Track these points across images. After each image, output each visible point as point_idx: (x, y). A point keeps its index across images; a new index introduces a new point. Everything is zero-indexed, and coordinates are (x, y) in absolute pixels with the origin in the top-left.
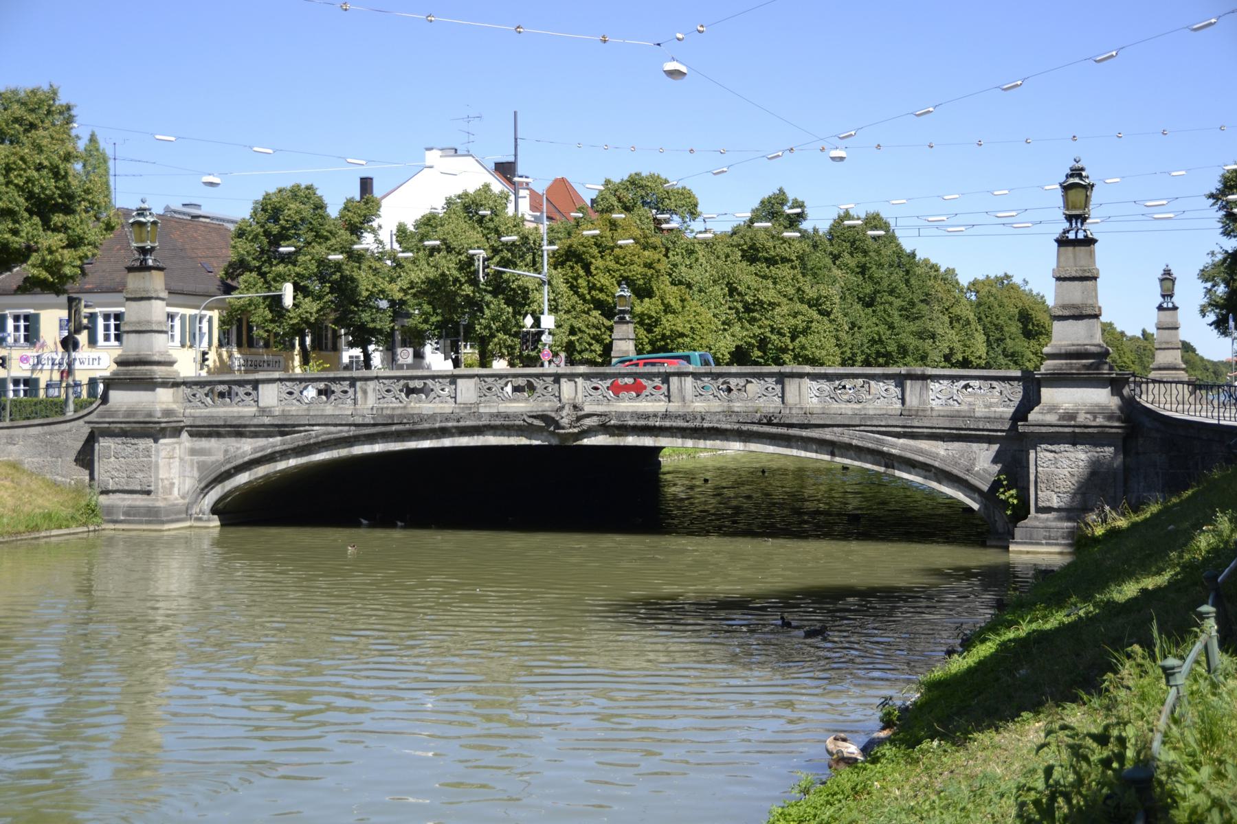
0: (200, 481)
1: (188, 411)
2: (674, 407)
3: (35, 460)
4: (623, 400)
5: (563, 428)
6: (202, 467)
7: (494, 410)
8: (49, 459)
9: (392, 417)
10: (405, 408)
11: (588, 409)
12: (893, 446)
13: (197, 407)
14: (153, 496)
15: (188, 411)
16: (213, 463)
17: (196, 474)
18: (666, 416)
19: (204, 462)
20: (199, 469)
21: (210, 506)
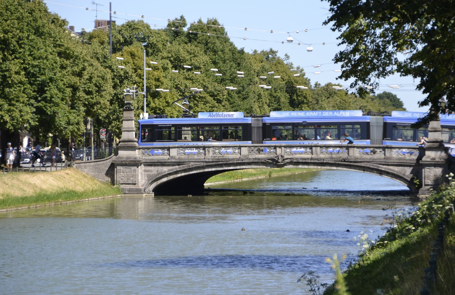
0: (148, 180)
1: (143, 157)
2: (314, 156)
3: (92, 173)
4: (261, 154)
5: (280, 163)
6: (148, 176)
7: (254, 157)
8: (97, 173)
9: (219, 159)
10: (223, 156)
11: (286, 157)
12: (382, 168)
13: (147, 156)
14: (136, 185)
15: (143, 157)
16: (153, 175)
17: (146, 178)
18: (312, 159)
19: (149, 174)
20: (147, 177)
21: (152, 189)
